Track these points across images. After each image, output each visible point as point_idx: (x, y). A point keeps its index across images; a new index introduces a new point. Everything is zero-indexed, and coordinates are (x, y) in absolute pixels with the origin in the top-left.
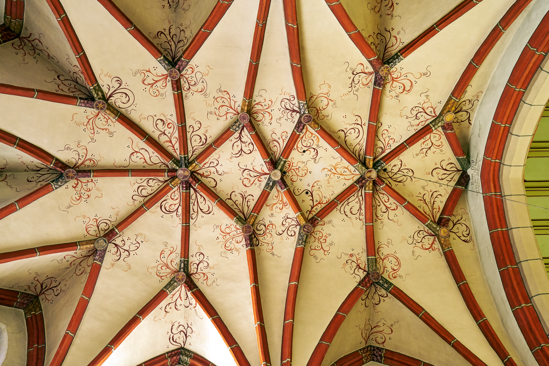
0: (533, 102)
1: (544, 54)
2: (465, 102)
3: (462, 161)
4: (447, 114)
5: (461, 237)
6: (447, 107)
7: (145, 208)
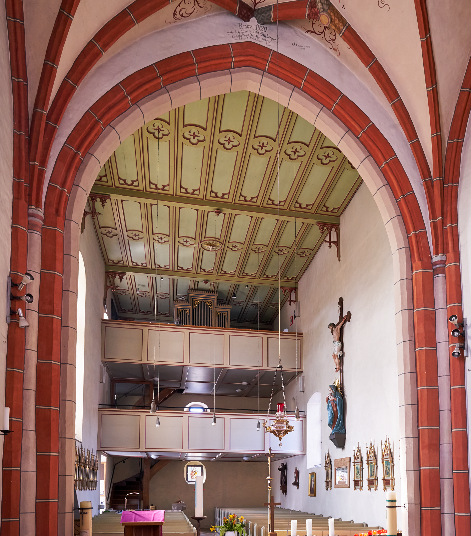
0: (319, 117)
1: (359, 136)
2: (334, 35)
3: (267, 14)
4: (329, 18)
5: (180, 6)
6: (336, 17)
7: (437, 179)
